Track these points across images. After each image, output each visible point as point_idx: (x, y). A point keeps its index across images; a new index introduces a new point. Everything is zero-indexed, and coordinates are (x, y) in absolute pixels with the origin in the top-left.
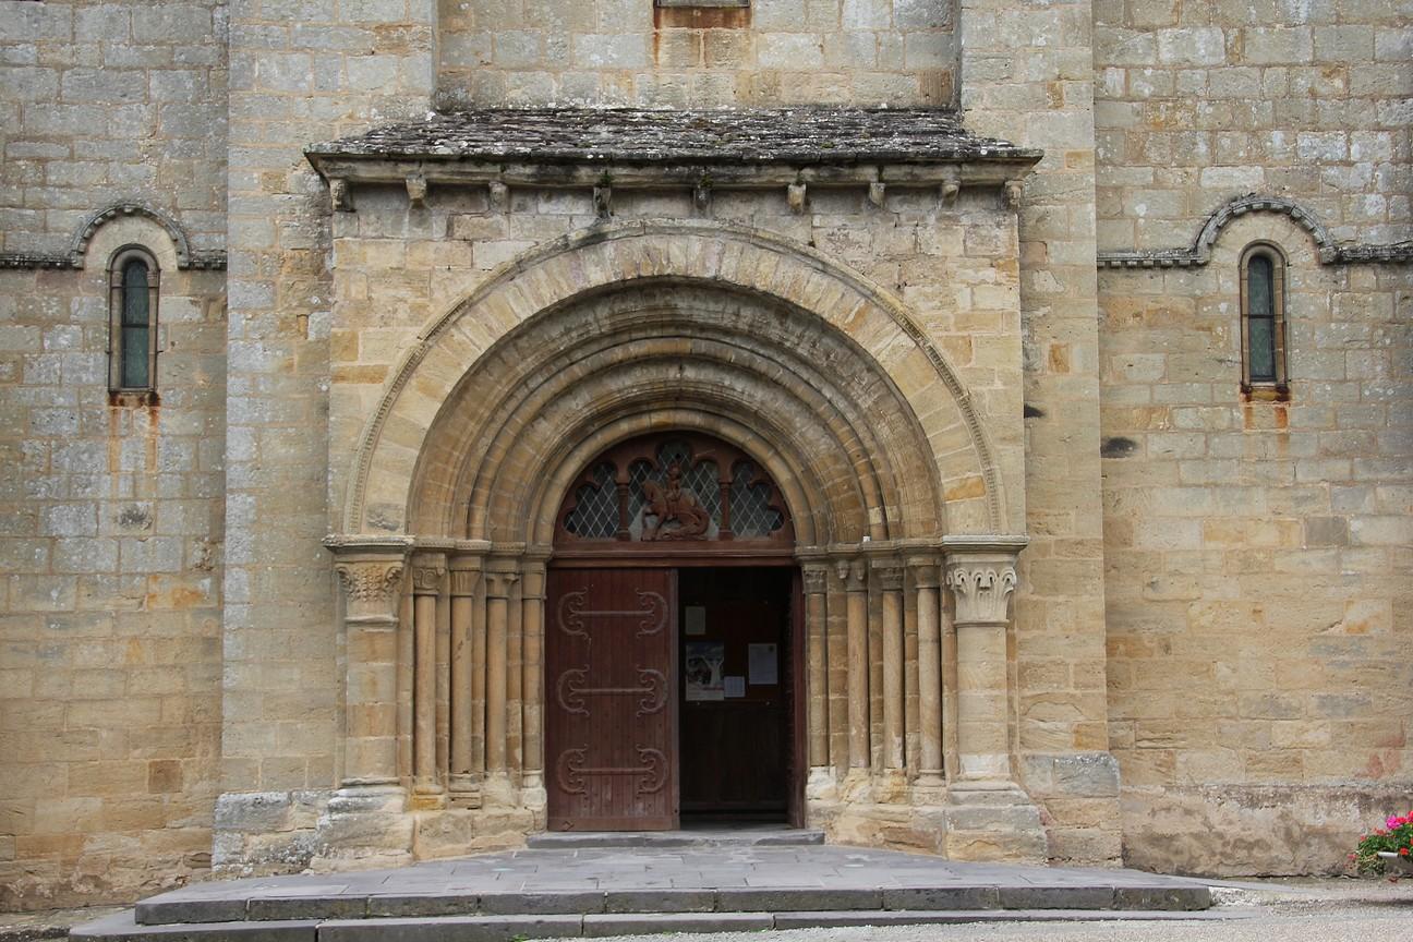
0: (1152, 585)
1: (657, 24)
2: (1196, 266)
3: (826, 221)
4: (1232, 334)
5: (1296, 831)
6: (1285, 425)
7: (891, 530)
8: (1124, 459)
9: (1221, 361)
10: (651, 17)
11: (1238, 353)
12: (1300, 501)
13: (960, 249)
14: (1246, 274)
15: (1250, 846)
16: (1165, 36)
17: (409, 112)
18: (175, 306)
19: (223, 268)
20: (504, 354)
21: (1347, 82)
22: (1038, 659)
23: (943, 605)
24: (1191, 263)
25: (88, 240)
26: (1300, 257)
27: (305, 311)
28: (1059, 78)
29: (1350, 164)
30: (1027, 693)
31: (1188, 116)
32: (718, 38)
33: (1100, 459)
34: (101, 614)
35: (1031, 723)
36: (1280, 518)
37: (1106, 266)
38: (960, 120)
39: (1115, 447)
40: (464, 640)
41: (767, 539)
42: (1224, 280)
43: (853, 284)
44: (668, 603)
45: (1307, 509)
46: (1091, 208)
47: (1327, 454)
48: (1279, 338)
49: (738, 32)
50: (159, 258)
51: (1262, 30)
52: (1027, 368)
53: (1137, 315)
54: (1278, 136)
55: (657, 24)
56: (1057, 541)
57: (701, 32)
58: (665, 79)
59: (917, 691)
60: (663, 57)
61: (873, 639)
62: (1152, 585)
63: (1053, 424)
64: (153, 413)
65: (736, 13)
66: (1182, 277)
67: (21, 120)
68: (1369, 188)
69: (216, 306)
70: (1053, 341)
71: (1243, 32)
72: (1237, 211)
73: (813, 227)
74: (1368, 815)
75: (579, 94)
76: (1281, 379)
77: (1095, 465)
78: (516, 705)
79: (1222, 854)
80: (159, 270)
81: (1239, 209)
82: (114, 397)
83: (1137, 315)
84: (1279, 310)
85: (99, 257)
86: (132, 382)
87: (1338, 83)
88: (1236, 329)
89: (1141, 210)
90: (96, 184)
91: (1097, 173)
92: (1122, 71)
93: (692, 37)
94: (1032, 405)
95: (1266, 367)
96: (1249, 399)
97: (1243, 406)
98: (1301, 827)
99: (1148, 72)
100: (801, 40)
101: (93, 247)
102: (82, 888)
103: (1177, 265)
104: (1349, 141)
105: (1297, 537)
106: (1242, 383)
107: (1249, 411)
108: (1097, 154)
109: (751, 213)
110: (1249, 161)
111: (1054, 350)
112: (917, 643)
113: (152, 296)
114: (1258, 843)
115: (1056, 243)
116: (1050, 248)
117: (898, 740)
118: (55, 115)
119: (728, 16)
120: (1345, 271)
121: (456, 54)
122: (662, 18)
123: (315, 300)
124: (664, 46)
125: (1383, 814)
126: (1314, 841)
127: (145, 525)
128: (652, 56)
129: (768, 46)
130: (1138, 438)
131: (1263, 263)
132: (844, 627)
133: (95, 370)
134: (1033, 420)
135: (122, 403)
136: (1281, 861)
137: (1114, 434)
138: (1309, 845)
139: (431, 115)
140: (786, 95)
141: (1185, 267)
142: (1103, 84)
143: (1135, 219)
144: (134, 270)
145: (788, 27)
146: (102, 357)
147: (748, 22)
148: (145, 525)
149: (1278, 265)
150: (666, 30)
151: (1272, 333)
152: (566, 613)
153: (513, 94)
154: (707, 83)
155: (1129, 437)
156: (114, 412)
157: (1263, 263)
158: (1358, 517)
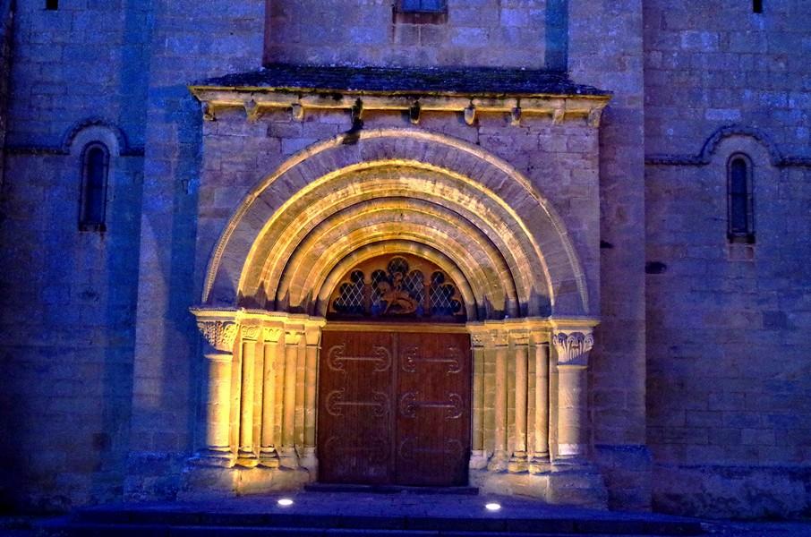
0: (674, 348)
1: (394, 21)
2: (700, 164)
3: (487, 131)
4: (722, 204)
5: (754, 493)
6: (752, 257)
7: (522, 312)
8: (661, 275)
9: (716, 220)
10: (391, 17)
11: (725, 215)
12: (760, 302)
13: (565, 148)
14: (730, 170)
15: (726, 502)
16: (685, 35)
17: (250, 66)
18: (115, 176)
19: (143, 154)
20: (605, 156)
21: (787, 64)
22: (604, 389)
23: (551, 355)
24: (699, 161)
25: (72, 138)
26: (763, 162)
27: (187, 178)
28: (624, 54)
29: (789, 110)
30: (599, 409)
31: (697, 79)
32: (429, 30)
33: (644, 274)
34: (70, 349)
35: (601, 426)
36: (748, 311)
37: (650, 161)
38: (567, 76)
39: (654, 268)
40: (271, 368)
41: (451, 317)
42: (718, 173)
43: (510, 384)
44: (392, 355)
45: (765, 307)
46: (641, 129)
47: (778, 275)
48: (749, 208)
49: (440, 26)
50: (110, 149)
51: (738, 34)
52: (603, 219)
53: (669, 191)
54: (748, 93)
55: (394, 21)
56: (570, 265)
57: (420, 26)
58: (398, 53)
59: (535, 406)
60: (397, 39)
61: (510, 375)
62: (674, 348)
63: (619, 251)
64: (102, 235)
65: (437, 14)
66: (694, 170)
67: (41, 73)
68: (801, 124)
69: (137, 173)
70: (619, 204)
71: (728, 34)
72: (726, 134)
73: (479, 134)
74: (794, 483)
75: (349, 60)
76: (750, 230)
77: (643, 276)
78: (301, 409)
79: (711, 506)
80: (109, 155)
81: (724, 131)
82: (82, 227)
83: (669, 191)
84: (749, 190)
85: (78, 144)
86: (91, 218)
87: (782, 65)
88: (725, 201)
89: (671, 131)
90: (77, 107)
91: (645, 110)
92: (661, 54)
93: (414, 28)
94: (606, 241)
95: (741, 224)
96: (731, 242)
97: (727, 245)
98: (757, 490)
99: (675, 55)
100: (477, 31)
101: (75, 142)
102: (56, 503)
103: (691, 163)
104: (788, 98)
105: (758, 323)
106: (728, 233)
107: (731, 248)
108: (645, 99)
109: (443, 124)
110: (732, 106)
111: (619, 209)
112: (535, 378)
113: (105, 169)
114: (732, 500)
115: (622, 148)
116: (618, 151)
117: (523, 435)
118: (59, 70)
119: (435, 18)
120: (786, 169)
121: (280, 36)
122: (398, 18)
123: (192, 172)
124: (398, 33)
125: (802, 483)
126: (764, 498)
127: (95, 299)
128: (390, 39)
129: (457, 34)
130: (668, 263)
131: (739, 167)
132: (493, 370)
133: (72, 210)
134: (607, 250)
135: (86, 230)
136: (745, 510)
137: (654, 259)
138: (761, 501)
139: (262, 69)
140: (467, 62)
141: (696, 165)
142: (649, 60)
143: (667, 138)
144: (95, 158)
145: (468, 22)
146: (76, 204)
147: (446, 20)
148: (95, 299)
149: (749, 165)
150: (399, 24)
151: (745, 205)
152: (333, 358)
153: (311, 59)
154: (422, 54)
155: (663, 262)
156: (81, 234)
157: (739, 167)
158: (793, 312)
